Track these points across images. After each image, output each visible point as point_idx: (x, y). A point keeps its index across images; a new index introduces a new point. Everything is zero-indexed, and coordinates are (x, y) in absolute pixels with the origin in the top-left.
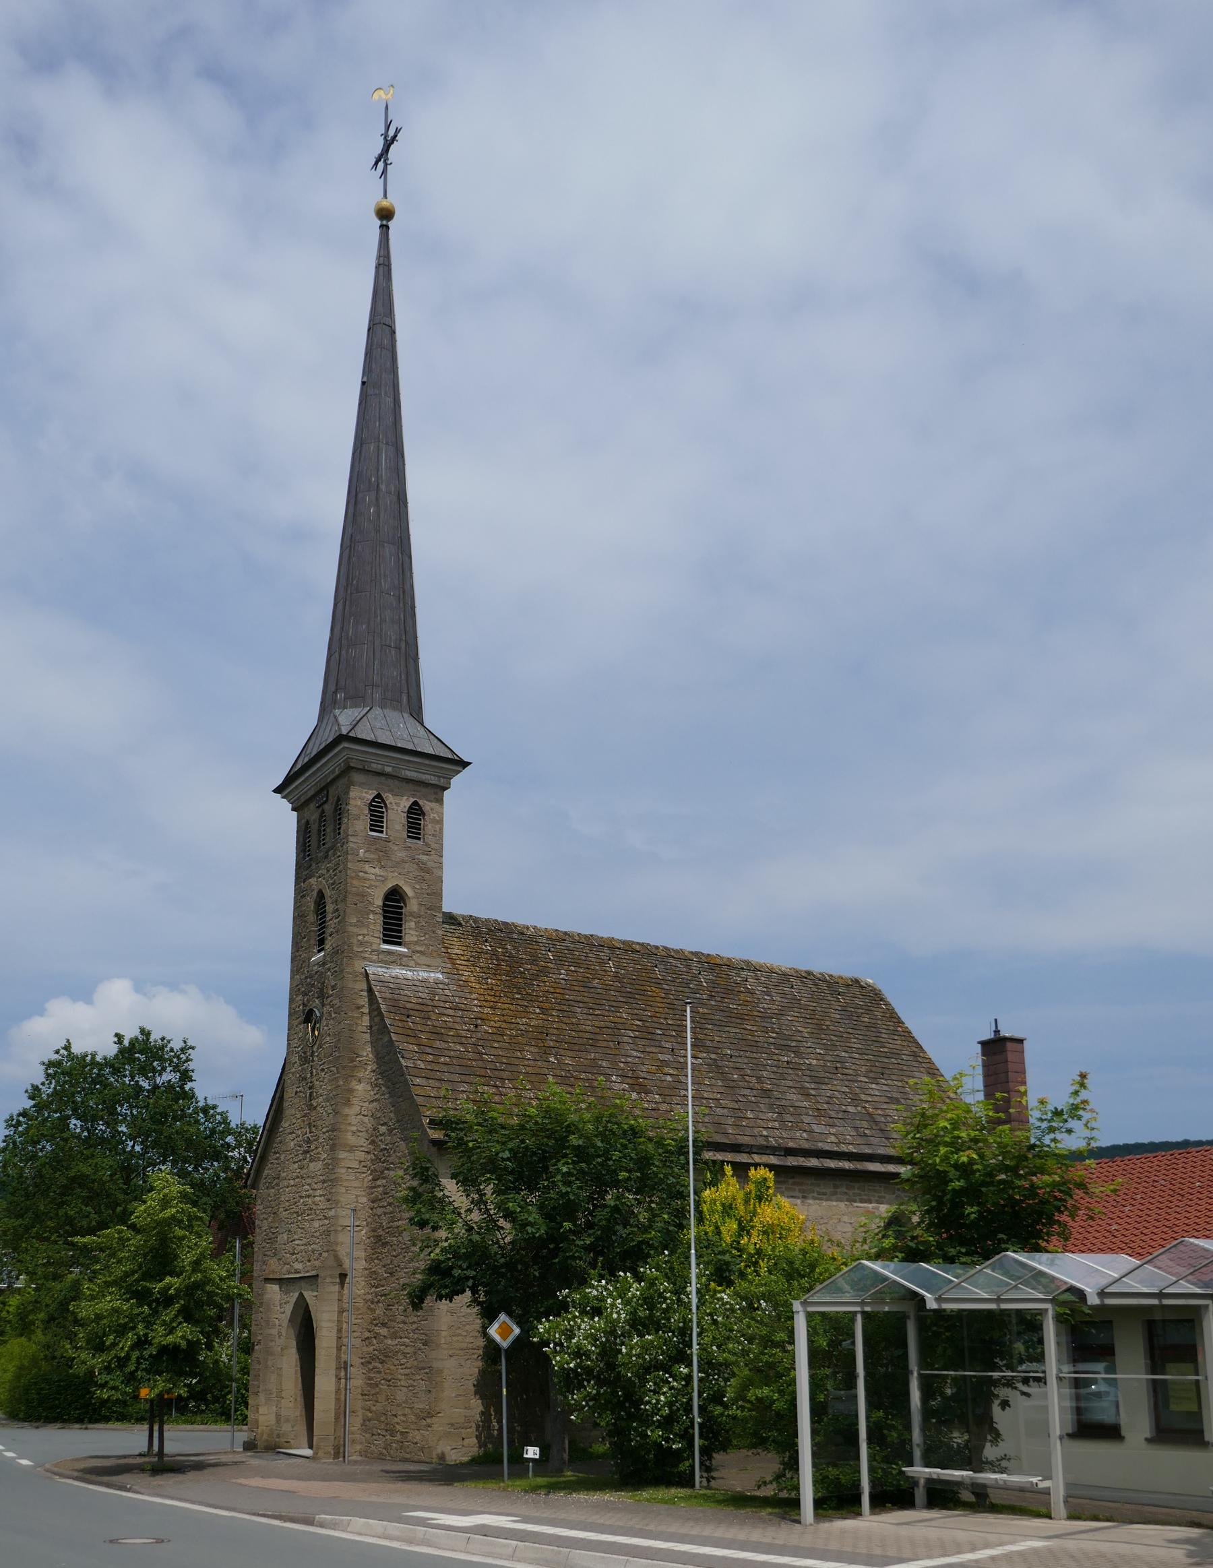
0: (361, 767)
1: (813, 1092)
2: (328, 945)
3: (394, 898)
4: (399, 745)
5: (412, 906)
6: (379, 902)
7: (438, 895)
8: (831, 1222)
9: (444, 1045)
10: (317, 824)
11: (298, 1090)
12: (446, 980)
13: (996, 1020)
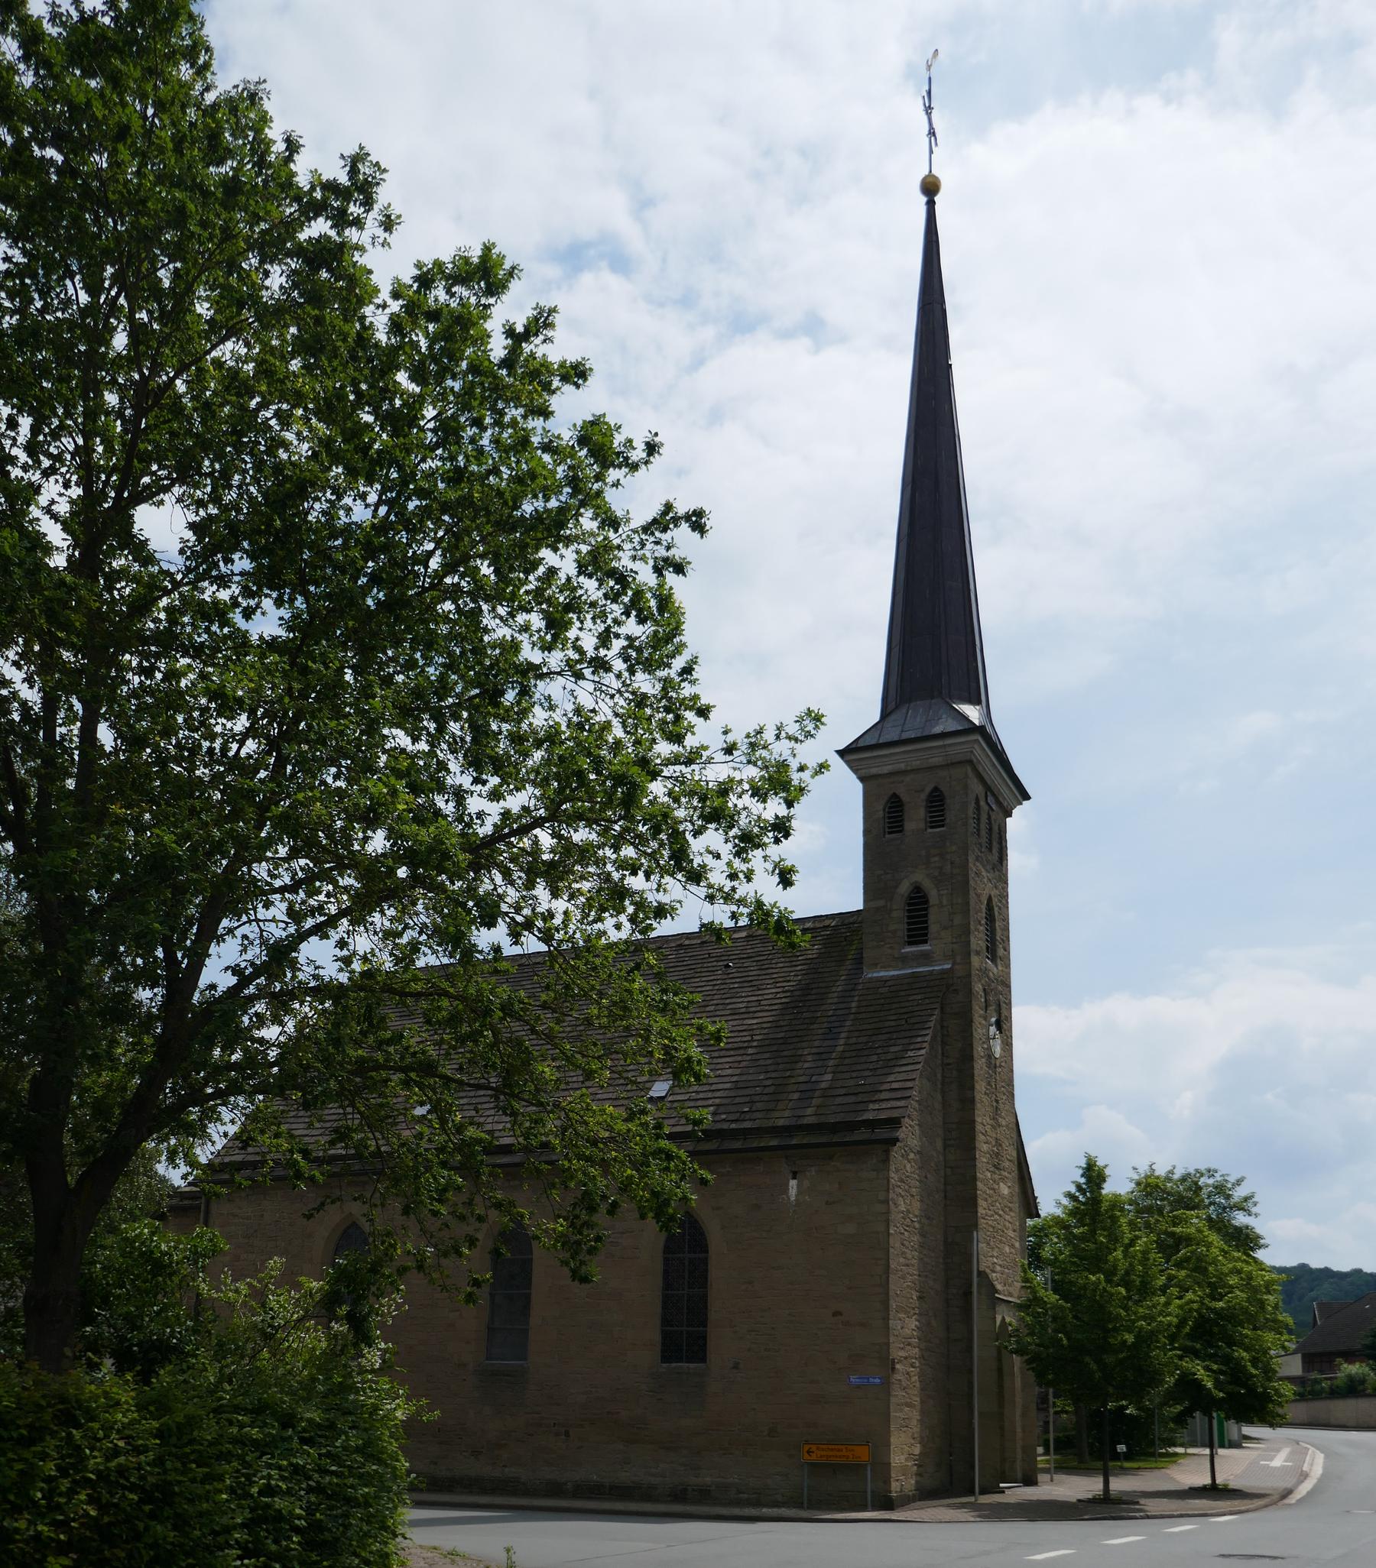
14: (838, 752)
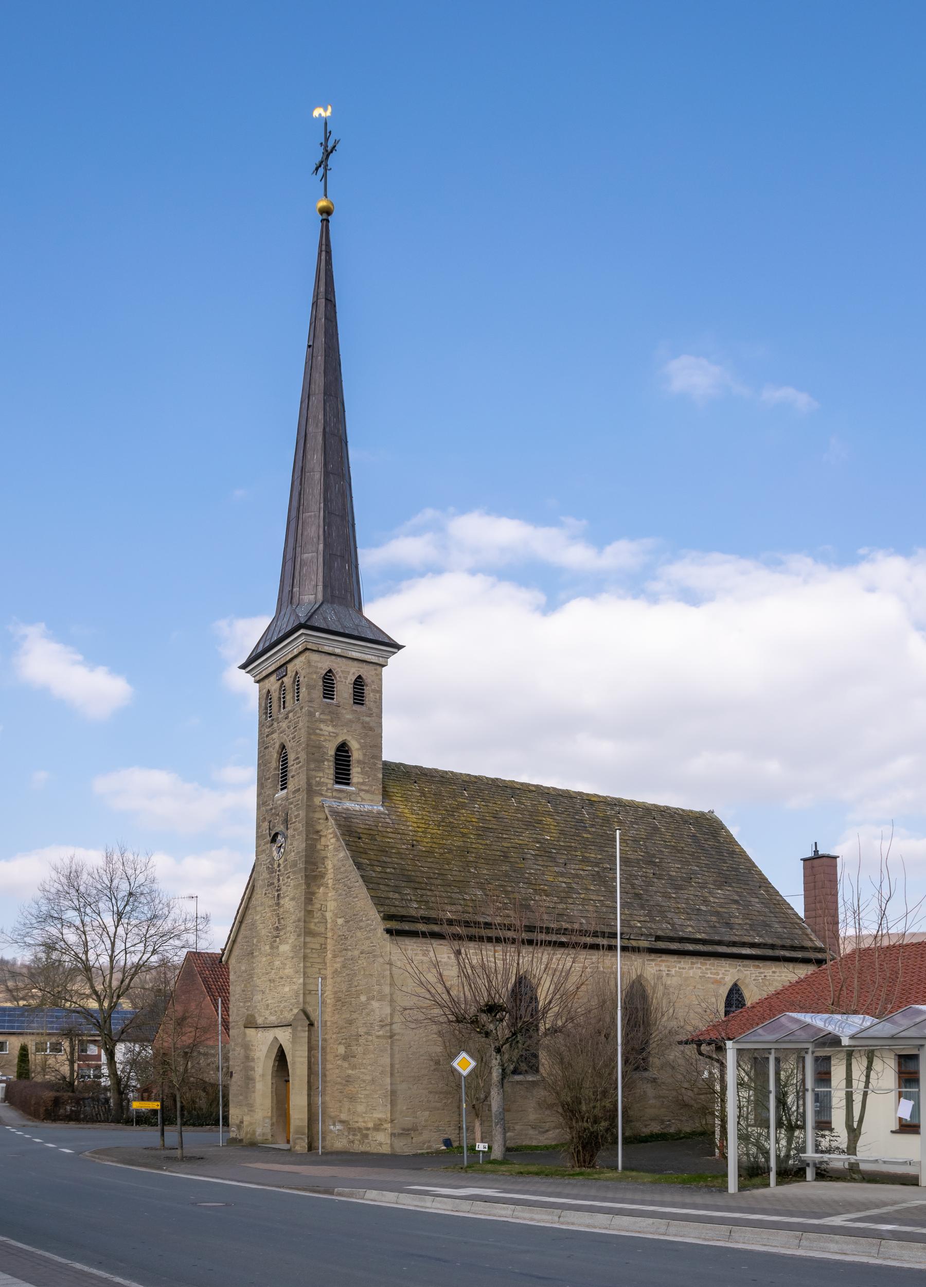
0: (316, 649)
1: (674, 896)
2: (292, 784)
3: (343, 751)
4: (347, 632)
5: (356, 754)
6: (332, 752)
7: (379, 747)
8: (688, 989)
9: (389, 860)
10: (277, 693)
11: (267, 892)
12: (386, 812)
13: (816, 843)
14: (243, 667)
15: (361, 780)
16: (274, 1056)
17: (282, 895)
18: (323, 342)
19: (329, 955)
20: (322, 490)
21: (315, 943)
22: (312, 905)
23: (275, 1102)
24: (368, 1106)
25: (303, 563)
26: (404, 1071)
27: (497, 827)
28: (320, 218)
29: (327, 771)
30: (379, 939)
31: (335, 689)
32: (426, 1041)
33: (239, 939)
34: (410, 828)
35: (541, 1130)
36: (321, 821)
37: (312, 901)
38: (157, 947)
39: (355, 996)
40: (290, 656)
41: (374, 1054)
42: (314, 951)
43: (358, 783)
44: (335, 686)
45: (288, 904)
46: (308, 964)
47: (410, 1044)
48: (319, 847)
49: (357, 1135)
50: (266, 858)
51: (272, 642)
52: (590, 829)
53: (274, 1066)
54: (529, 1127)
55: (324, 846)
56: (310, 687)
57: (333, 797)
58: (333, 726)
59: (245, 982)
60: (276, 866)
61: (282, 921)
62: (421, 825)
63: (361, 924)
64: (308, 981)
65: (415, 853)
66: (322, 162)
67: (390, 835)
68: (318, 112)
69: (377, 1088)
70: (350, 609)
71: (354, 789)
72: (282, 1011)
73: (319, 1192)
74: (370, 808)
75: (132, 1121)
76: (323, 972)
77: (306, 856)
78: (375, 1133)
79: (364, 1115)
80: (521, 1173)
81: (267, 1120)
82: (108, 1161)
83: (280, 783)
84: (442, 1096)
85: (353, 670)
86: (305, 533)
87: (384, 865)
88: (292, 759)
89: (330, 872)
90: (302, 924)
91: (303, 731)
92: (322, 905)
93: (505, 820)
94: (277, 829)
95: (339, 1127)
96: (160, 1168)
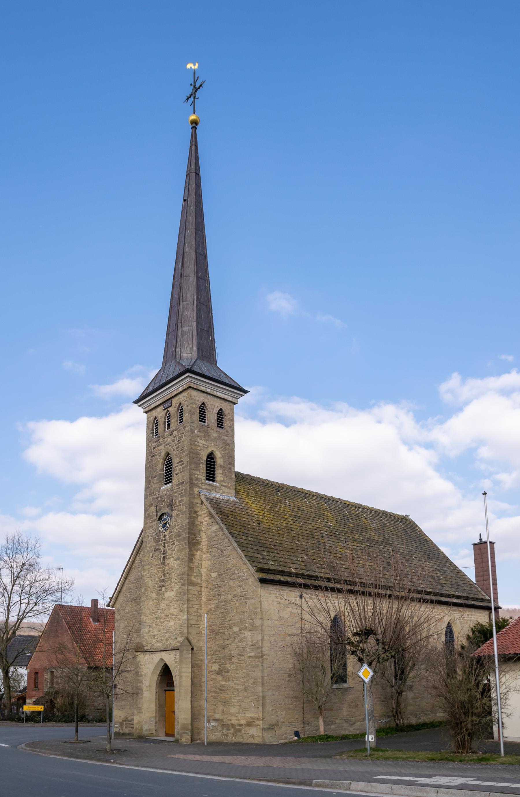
0: (195, 387)
2: (176, 480)
3: (211, 457)
5: (219, 461)
6: (205, 458)
10: (163, 419)
11: (154, 555)
12: (238, 501)
13: (480, 534)
14: (136, 402)
15: (222, 479)
16: (158, 672)
17: (167, 557)
18: (194, 198)
19: (204, 599)
20: (195, 288)
21: (194, 590)
22: (193, 563)
23: (158, 705)
24: (240, 708)
25: (183, 333)
26: (270, 681)
27: (302, 516)
28: (191, 126)
29: (202, 471)
30: (250, 586)
31: (206, 416)
32: (283, 660)
33: (123, 590)
34: (255, 513)
35: (350, 723)
36: (198, 505)
37: (192, 560)
38: (38, 600)
39: (228, 628)
40: (176, 393)
41: (246, 669)
42: (194, 596)
43: (220, 481)
44: (206, 414)
45: (172, 562)
46: (190, 606)
47: (273, 662)
48: (197, 523)
49: (230, 730)
50: (153, 531)
51: (160, 384)
52: (351, 521)
53: (158, 679)
54: (344, 721)
55: (200, 522)
56: (191, 413)
57: (206, 489)
58: (206, 440)
59: (128, 621)
60: (162, 537)
61: (167, 575)
62: (260, 511)
63: (234, 576)
64: (191, 617)
65: (262, 529)
66: (192, 95)
67: (244, 516)
68: (189, 66)
69: (249, 695)
70: (213, 365)
71: (218, 484)
72: (167, 640)
73: (293, 783)
74: (228, 498)
75: (23, 719)
76: (199, 611)
77: (189, 529)
78: (247, 728)
79: (237, 715)
80: (434, 760)
81: (152, 719)
82: (51, 754)
83: (164, 480)
84: (293, 700)
85: (217, 405)
86: (184, 314)
87: (246, 535)
88: (176, 462)
89: (204, 540)
90: (186, 577)
91: (186, 442)
92: (199, 563)
93: (305, 512)
94: (163, 511)
95: (213, 724)
96: (108, 761)
